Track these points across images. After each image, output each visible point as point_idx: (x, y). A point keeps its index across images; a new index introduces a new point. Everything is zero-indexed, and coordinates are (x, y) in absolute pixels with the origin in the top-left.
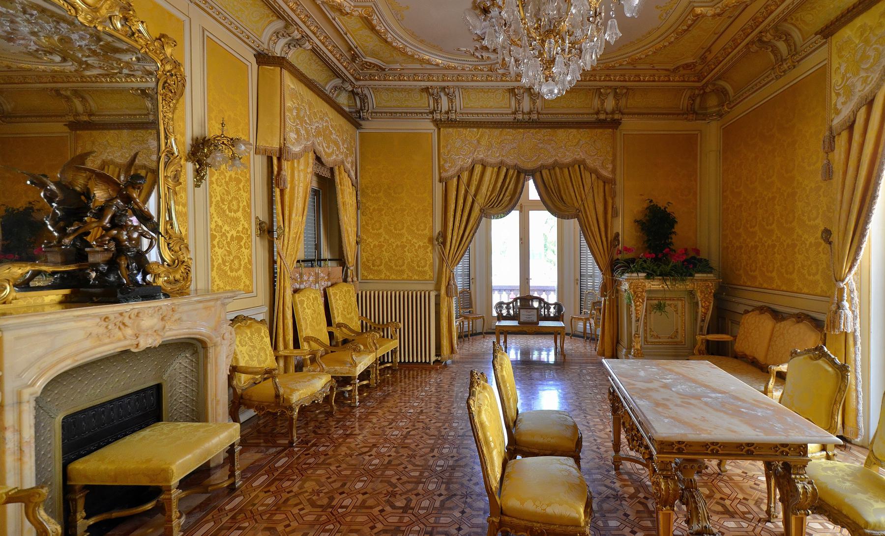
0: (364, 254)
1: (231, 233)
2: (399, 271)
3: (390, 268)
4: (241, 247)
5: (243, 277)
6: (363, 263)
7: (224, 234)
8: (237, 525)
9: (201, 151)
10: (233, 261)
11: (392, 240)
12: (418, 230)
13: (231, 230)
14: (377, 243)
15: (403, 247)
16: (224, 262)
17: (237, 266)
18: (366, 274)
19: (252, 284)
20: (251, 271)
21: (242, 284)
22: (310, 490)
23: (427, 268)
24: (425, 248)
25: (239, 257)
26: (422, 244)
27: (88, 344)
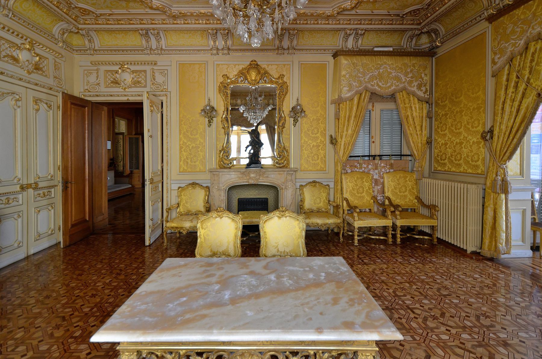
0: (436, 151)
1: (192, 145)
2: (474, 166)
3: (451, 162)
4: (447, 148)
5: (463, 164)
6: (435, 158)
7: (468, 141)
8: (527, 331)
9: (297, 112)
10: (456, 155)
11: (189, 143)
12: (312, 134)
13: (473, 138)
14: (194, 145)
15: (461, 143)
16: (452, 156)
17: (459, 158)
18: (436, 166)
19: (325, 167)
20: (325, 161)
21: (462, 168)
22: (435, 321)
23: (479, 163)
24: (478, 143)
25: (460, 153)
26: (315, 144)
27: (237, 179)
